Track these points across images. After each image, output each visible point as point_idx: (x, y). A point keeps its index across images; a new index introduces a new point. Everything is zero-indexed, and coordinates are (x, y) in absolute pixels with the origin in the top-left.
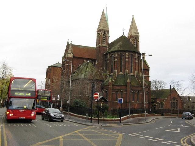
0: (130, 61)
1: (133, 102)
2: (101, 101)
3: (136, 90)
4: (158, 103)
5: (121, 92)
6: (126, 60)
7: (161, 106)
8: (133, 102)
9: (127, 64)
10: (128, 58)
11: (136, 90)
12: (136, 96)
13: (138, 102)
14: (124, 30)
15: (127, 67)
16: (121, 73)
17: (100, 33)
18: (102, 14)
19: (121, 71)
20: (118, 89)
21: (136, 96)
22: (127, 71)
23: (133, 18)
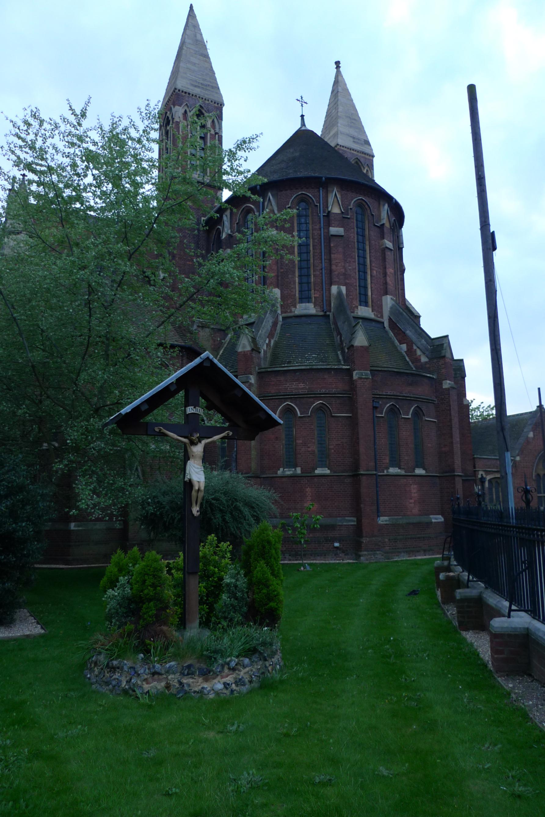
0: (353, 236)
1: (393, 470)
2: (192, 428)
3: (409, 401)
4: (482, 480)
5: (321, 409)
6: (334, 230)
7: (498, 497)
8: (393, 470)
9: (337, 257)
10: (343, 220)
11: (409, 401)
12: (406, 433)
13: (419, 471)
14: (302, 101)
15: (338, 269)
16: (310, 309)
17: (178, 111)
18: (189, 15)
19: (305, 298)
20: (296, 397)
21: (406, 433)
22: (340, 293)
23: (338, 74)
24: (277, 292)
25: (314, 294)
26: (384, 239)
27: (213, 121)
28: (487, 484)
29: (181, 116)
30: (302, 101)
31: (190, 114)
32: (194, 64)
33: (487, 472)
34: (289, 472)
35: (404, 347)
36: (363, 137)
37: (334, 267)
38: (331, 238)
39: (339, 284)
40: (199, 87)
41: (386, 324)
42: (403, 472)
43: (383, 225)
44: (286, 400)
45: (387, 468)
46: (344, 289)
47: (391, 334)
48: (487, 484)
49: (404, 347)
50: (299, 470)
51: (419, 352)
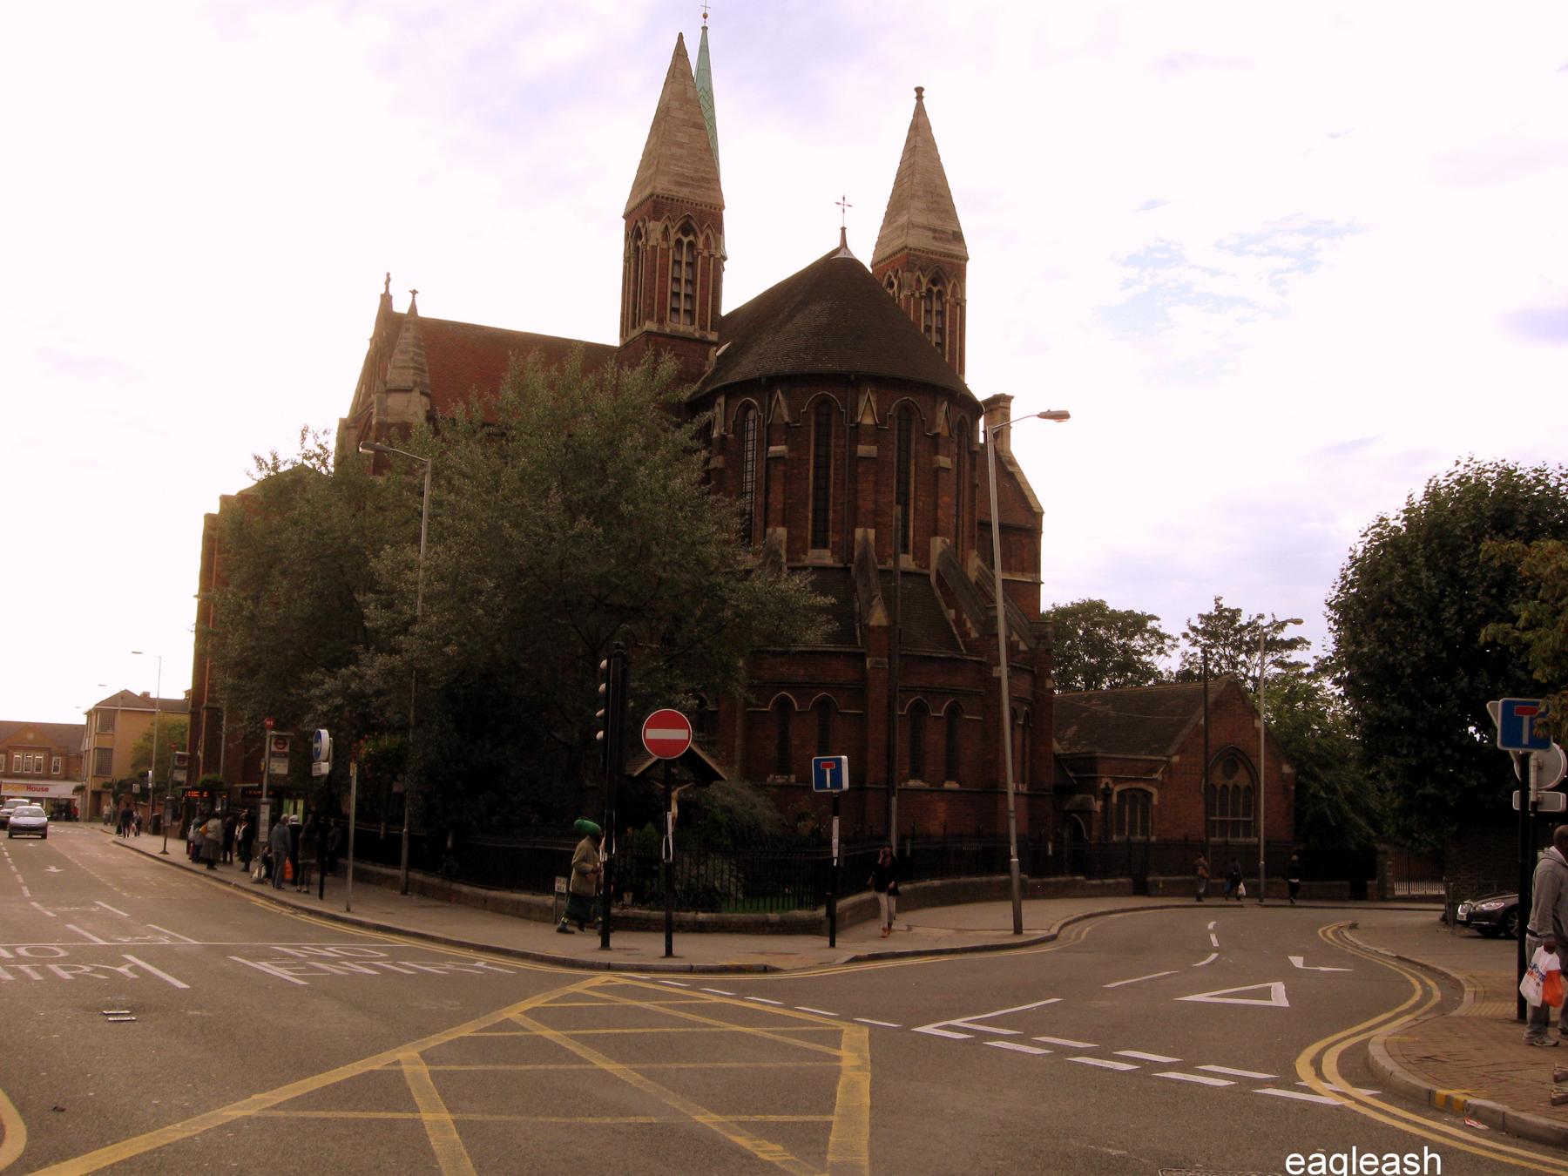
1: (912, 783)
4: (1107, 794)
5: (824, 704)
6: (864, 450)
8: (912, 783)
10: (877, 434)
12: (935, 738)
13: (951, 785)
14: (844, 204)
19: (820, 542)
21: (935, 738)
22: (866, 538)
23: (920, 111)
24: (782, 532)
25: (832, 537)
26: (937, 453)
27: (707, 237)
28: (1114, 799)
29: (659, 236)
30: (844, 204)
31: (672, 232)
32: (681, 146)
33: (1117, 781)
34: (780, 780)
35: (952, 613)
36: (949, 228)
37: (860, 502)
38: (856, 460)
39: (866, 527)
40: (686, 185)
41: (933, 579)
42: (927, 786)
43: (938, 435)
44: (782, 689)
45: (906, 781)
46: (872, 533)
47: (938, 592)
48: (1114, 799)
49: (952, 613)
50: (793, 778)
51: (969, 624)
